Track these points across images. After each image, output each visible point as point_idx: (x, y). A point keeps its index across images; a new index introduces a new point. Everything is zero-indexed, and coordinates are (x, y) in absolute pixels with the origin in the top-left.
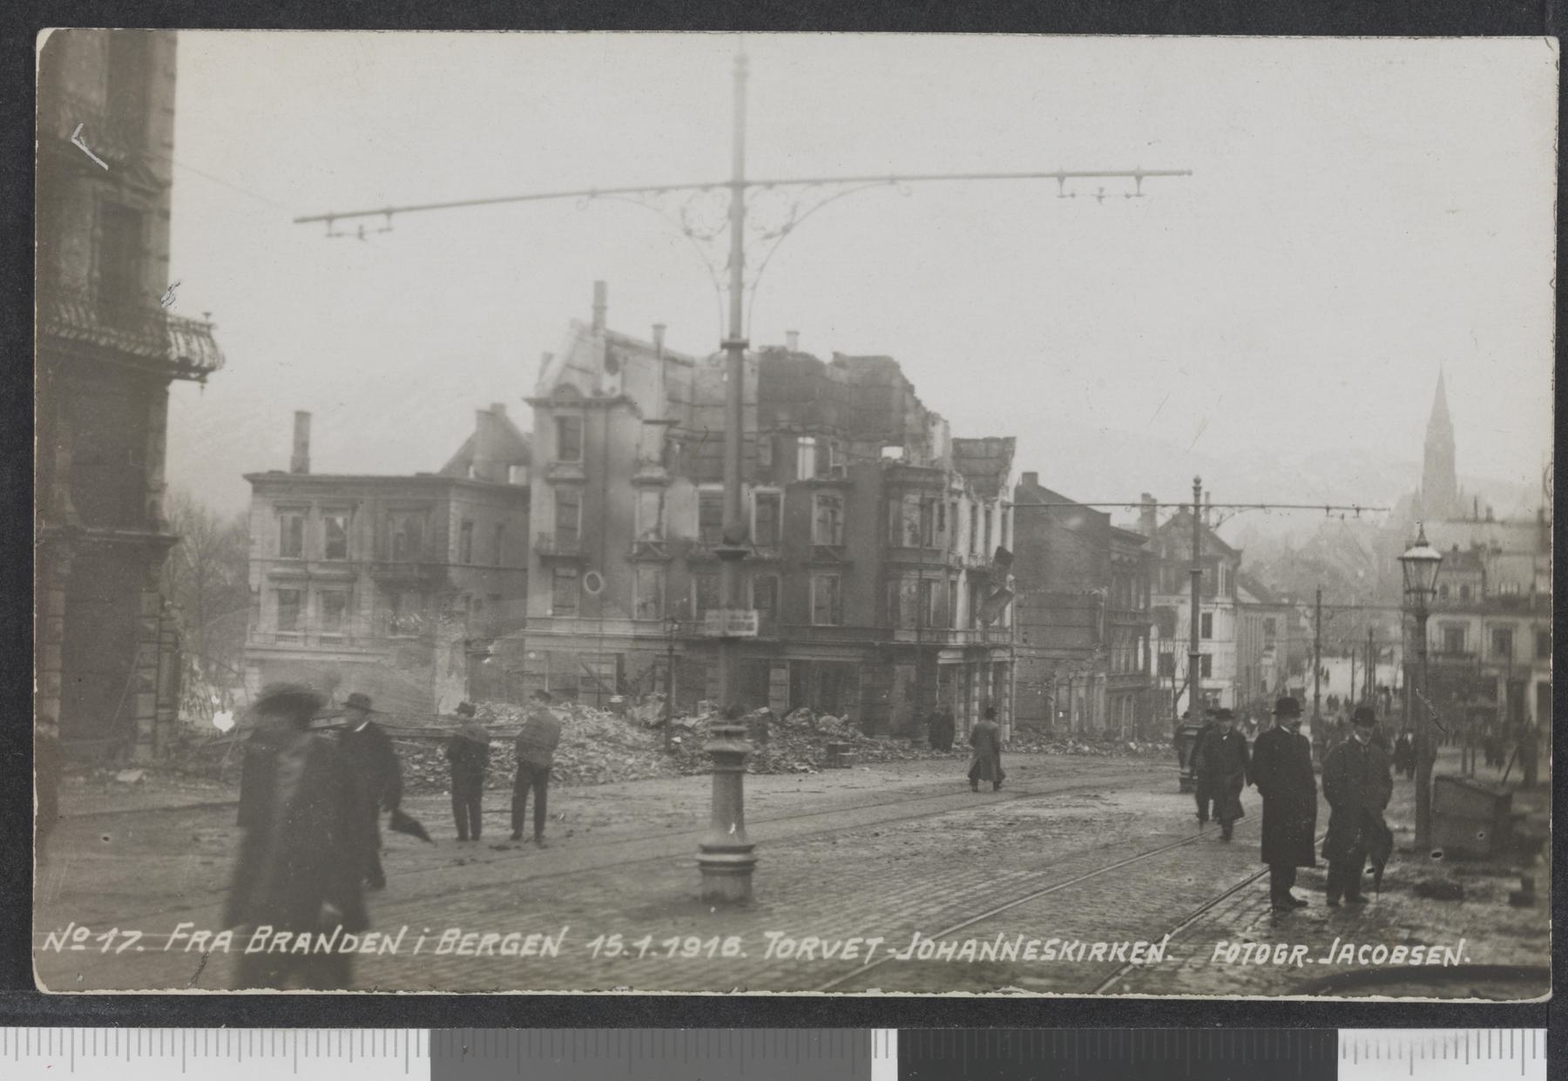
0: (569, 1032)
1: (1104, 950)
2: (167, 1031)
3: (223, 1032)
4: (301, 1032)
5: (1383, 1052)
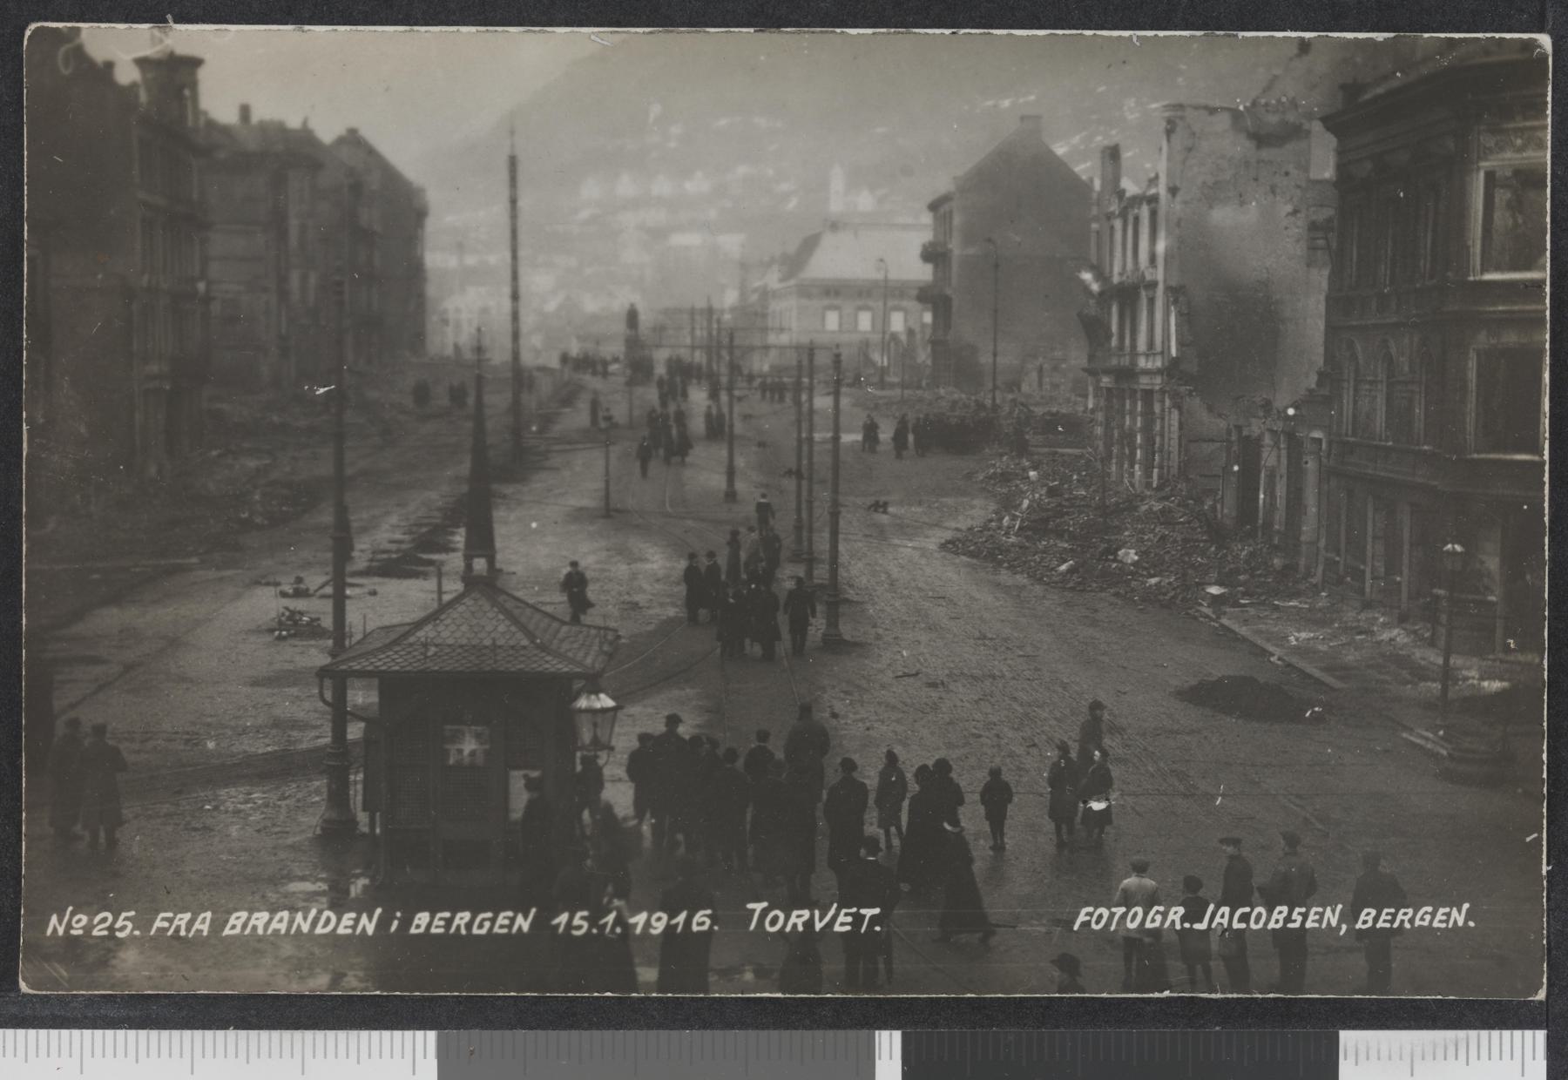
0: (575, 1033)
1: (243, 920)
2: (176, 1033)
3: (231, 1033)
4: (309, 1034)
5: (1385, 1053)
